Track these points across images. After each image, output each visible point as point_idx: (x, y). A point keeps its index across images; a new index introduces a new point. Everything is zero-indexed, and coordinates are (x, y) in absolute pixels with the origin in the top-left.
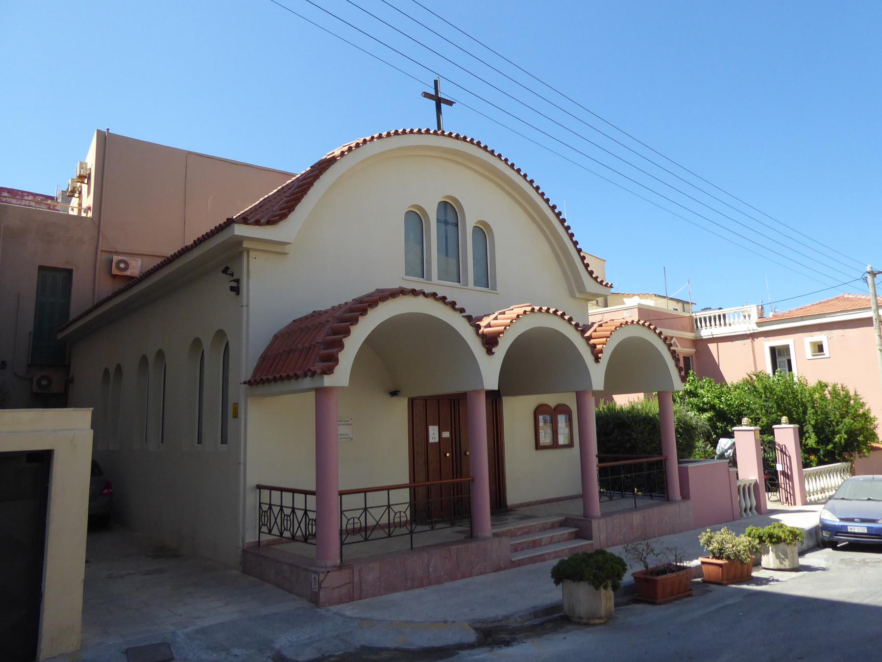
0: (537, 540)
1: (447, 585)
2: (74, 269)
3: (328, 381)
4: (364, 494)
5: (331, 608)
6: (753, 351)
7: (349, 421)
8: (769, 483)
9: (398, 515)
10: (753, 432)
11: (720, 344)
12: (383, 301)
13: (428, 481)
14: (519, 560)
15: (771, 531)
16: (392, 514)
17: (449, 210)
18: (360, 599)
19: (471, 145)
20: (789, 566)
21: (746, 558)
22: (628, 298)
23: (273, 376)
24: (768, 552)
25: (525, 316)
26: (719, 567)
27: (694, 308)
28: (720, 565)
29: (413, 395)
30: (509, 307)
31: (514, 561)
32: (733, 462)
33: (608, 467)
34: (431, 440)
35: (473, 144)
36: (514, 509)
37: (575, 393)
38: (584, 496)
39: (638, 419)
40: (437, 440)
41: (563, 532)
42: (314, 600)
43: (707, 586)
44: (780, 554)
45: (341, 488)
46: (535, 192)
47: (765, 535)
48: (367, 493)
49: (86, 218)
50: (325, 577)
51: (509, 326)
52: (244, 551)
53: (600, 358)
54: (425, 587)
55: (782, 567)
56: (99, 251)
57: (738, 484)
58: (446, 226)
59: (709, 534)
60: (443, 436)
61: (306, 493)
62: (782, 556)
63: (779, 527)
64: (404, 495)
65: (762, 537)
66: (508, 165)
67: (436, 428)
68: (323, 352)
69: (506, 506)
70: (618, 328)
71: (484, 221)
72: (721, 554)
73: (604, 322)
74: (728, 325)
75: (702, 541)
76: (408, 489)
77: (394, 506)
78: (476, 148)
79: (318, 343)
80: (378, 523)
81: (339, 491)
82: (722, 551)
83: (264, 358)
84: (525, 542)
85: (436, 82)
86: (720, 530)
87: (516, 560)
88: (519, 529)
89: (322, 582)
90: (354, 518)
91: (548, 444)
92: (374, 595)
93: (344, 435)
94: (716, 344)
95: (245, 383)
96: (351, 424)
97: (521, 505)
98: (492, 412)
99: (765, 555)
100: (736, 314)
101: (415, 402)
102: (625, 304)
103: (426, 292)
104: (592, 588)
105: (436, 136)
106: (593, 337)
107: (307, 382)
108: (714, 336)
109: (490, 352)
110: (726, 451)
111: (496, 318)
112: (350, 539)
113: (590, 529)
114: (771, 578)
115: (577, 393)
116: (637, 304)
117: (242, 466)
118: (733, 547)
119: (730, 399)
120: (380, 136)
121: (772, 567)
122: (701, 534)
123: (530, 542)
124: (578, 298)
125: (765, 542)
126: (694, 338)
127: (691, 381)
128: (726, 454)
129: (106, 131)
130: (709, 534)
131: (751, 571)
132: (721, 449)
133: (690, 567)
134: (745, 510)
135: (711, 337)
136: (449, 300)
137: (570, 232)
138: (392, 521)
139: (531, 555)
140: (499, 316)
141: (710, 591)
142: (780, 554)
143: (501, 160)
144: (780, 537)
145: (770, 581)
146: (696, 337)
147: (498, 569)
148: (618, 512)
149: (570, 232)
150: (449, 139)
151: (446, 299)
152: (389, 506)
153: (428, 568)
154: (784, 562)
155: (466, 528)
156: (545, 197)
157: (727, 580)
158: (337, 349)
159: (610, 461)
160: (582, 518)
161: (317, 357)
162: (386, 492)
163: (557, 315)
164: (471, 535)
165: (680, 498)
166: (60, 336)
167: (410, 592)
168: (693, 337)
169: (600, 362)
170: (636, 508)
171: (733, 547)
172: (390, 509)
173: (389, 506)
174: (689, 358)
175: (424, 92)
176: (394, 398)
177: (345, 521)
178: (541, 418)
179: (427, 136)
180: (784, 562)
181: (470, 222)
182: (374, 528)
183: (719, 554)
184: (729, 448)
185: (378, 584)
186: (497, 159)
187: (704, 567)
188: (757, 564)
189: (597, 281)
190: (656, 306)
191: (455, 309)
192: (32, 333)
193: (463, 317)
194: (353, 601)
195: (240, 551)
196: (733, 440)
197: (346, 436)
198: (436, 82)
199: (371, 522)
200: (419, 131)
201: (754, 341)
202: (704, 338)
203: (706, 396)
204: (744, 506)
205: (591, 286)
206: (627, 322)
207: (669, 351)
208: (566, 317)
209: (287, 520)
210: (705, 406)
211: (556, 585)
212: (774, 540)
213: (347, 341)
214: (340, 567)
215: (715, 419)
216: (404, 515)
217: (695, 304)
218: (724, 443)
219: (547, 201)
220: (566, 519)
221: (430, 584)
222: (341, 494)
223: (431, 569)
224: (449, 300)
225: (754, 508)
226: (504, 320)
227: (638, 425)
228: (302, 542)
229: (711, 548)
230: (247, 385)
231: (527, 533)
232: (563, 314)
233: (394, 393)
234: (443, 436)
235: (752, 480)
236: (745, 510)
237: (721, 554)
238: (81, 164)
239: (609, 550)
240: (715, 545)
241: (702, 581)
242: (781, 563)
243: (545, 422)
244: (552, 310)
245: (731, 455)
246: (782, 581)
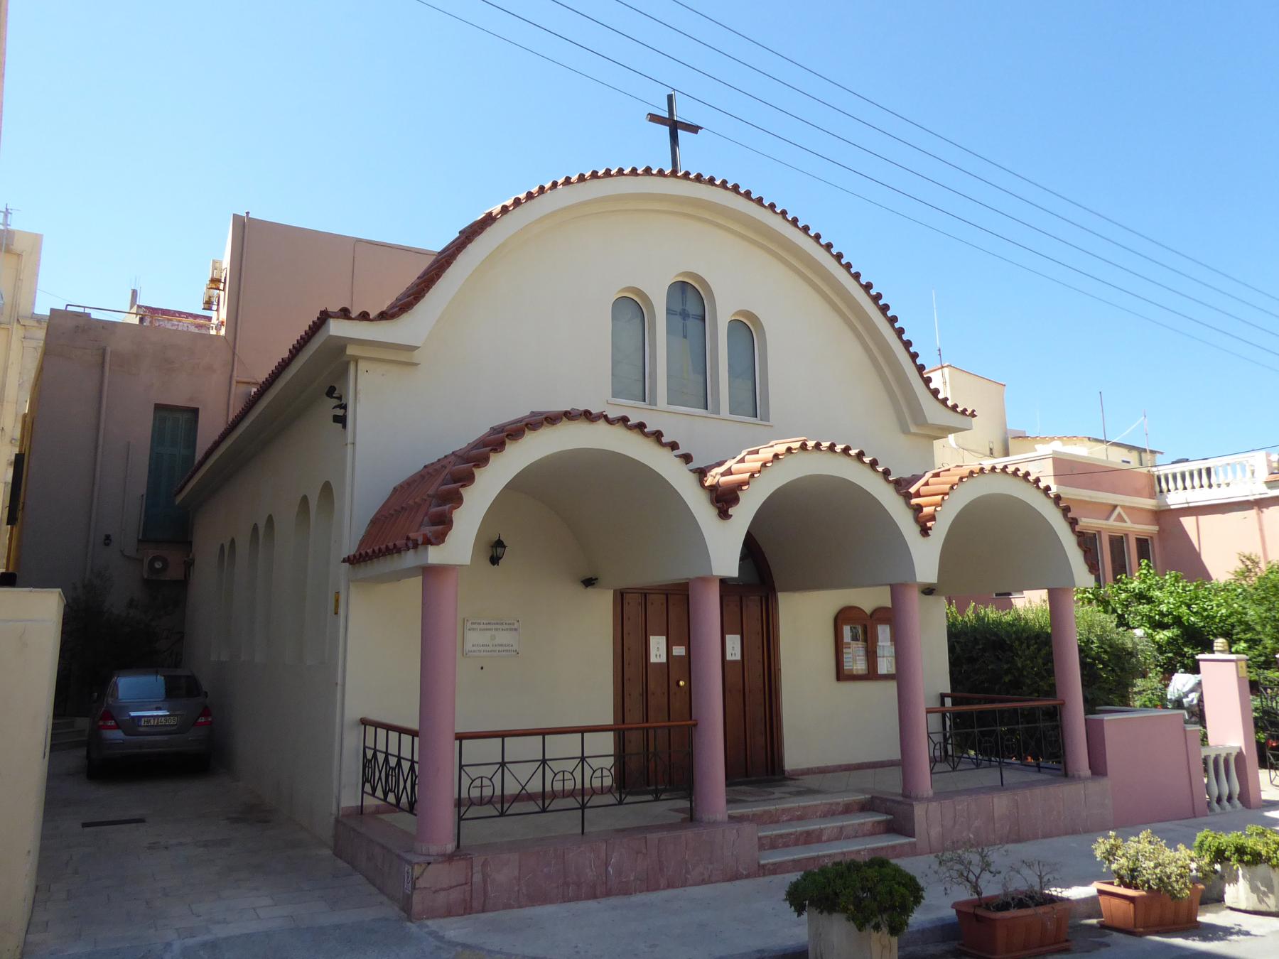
0: (813, 831)
1: (638, 898)
2: (200, 407)
3: (435, 555)
4: (541, 737)
5: (429, 923)
6: (1261, 530)
7: (513, 624)
8: (1272, 754)
9: (560, 777)
10: (1233, 664)
11: (1201, 518)
12: (534, 430)
13: (647, 721)
14: (774, 864)
15: (1241, 841)
16: (549, 775)
17: (690, 293)
18: (483, 911)
19: (722, 191)
20: (1276, 906)
21: (1181, 889)
22: (1043, 443)
23: (371, 550)
24: (1236, 880)
25: (791, 456)
26: (1128, 902)
27: (1158, 458)
28: (1131, 899)
29: (623, 584)
30: (769, 443)
31: (764, 866)
32: (1198, 714)
33: (972, 712)
34: (653, 659)
35: (727, 188)
36: (796, 777)
37: (888, 588)
38: (904, 763)
39: (1025, 635)
40: (664, 660)
41: (862, 821)
42: (406, 908)
43: (1106, 936)
44: (1259, 885)
45: (460, 729)
46: (835, 263)
47: (1229, 848)
48: (464, 742)
49: (217, 336)
50: (423, 872)
51: (759, 472)
52: (337, 821)
53: (930, 528)
54: (599, 900)
55: (1263, 908)
56: (234, 382)
57: (1205, 752)
58: (684, 319)
59: (1112, 841)
60: (674, 654)
61: (401, 731)
62: (1263, 889)
63: (1257, 834)
64: (605, 743)
65: (1225, 850)
66: (788, 221)
68: (434, 510)
69: (783, 771)
70: (964, 480)
71: (748, 311)
72: (1133, 878)
73: (943, 469)
74: (1215, 487)
75: (1099, 854)
76: (611, 734)
77: (590, 759)
78: (731, 195)
79: (429, 496)
80: (523, 788)
81: (456, 734)
82: (1136, 874)
83: (374, 522)
84: (791, 834)
85: (670, 98)
86: (1137, 835)
87: (768, 864)
88: (784, 811)
89: (418, 878)
90: (482, 778)
91: (860, 672)
92: (508, 906)
94: (1194, 518)
95: (344, 561)
96: (516, 630)
97: (809, 772)
98: (760, 618)
99: (1232, 885)
100: (1229, 468)
101: (627, 598)
102: (1036, 451)
103: (609, 416)
104: (852, 926)
105: (662, 178)
106: (922, 494)
107: (410, 559)
108: (1191, 505)
109: (724, 514)
110: (1186, 695)
111: (742, 461)
112: (473, 812)
113: (910, 818)
114: (1237, 928)
115: (892, 586)
116: (1051, 452)
117: (339, 687)
118: (1156, 867)
119: (1209, 607)
120: (568, 181)
121: (1243, 907)
122: (1095, 841)
123: (801, 833)
124: (915, 434)
125: (1230, 861)
126: (1154, 508)
127: (1142, 576)
128: (1185, 700)
129: (245, 215)
130: (1112, 841)
131: (1197, 912)
132: (1176, 691)
133: (1068, 899)
134: (1219, 800)
135: (1186, 505)
137: (897, 325)
138: (548, 788)
139: (796, 857)
140: (748, 458)
141: (1108, 945)
142: (1259, 885)
143: (775, 212)
144: (1259, 854)
145: (1232, 934)
146: (1159, 507)
147: (736, 877)
148: (969, 792)
149: (897, 325)
150: (685, 182)
151: (645, 427)
152: (583, 759)
153: (607, 868)
154: (1266, 899)
155: (685, 804)
156: (853, 270)
157: (1144, 928)
158: (450, 505)
159: (979, 703)
160: (900, 799)
161: (426, 518)
162: (500, 740)
163: (850, 455)
164: (691, 818)
165: (1089, 773)
166: (179, 499)
167: (572, 905)
168: (1153, 506)
169: (929, 535)
170: (1002, 786)
171: (1156, 867)
172: (585, 763)
173: (544, 762)
174: (1146, 540)
175: (649, 114)
176: (590, 589)
177: (466, 782)
178: (847, 630)
179: (647, 178)
180: (1266, 899)
181: (724, 312)
182: (517, 798)
183: (1130, 878)
184: (1192, 691)
185: (516, 889)
186: (769, 213)
187: (1102, 899)
188: (1215, 899)
189: (947, 406)
190: (1090, 455)
191: (663, 445)
192: (145, 497)
193: (676, 456)
194: (470, 914)
195: (332, 820)
196: (1198, 677)
197: (508, 648)
198: (670, 98)
199: (512, 788)
200: (620, 172)
201: (1262, 512)
202: (1172, 507)
203: (1166, 601)
204: (1215, 792)
205: (934, 413)
206: (972, 473)
207: (1066, 520)
208: (867, 460)
209: (392, 775)
210: (1166, 620)
211: (799, 916)
212: (1246, 858)
213: (468, 494)
214: (450, 858)
215: (1181, 641)
216: (571, 777)
217: (1162, 453)
218: (1181, 682)
219: (857, 276)
220: (872, 797)
221: (608, 894)
222: (460, 737)
223: (610, 869)
225: (1236, 796)
226: (753, 463)
227: (1024, 646)
228: (406, 811)
229: (1114, 867)
230: (347, 564)
231: (800, 818)
232: (860, 455)
233: (589, 582)
234: (674, 654)
235: (1232, 748)
236: (1219, 800)
237: (1133, 878)
238: (214, 262)
239: (893, 861)
240: (1121, 863)
241: (1099, 926)
242: (1261, 901)
243: (855, 638)
244: (839, 448)
245: (1195, 702)
246: (1256, 936)
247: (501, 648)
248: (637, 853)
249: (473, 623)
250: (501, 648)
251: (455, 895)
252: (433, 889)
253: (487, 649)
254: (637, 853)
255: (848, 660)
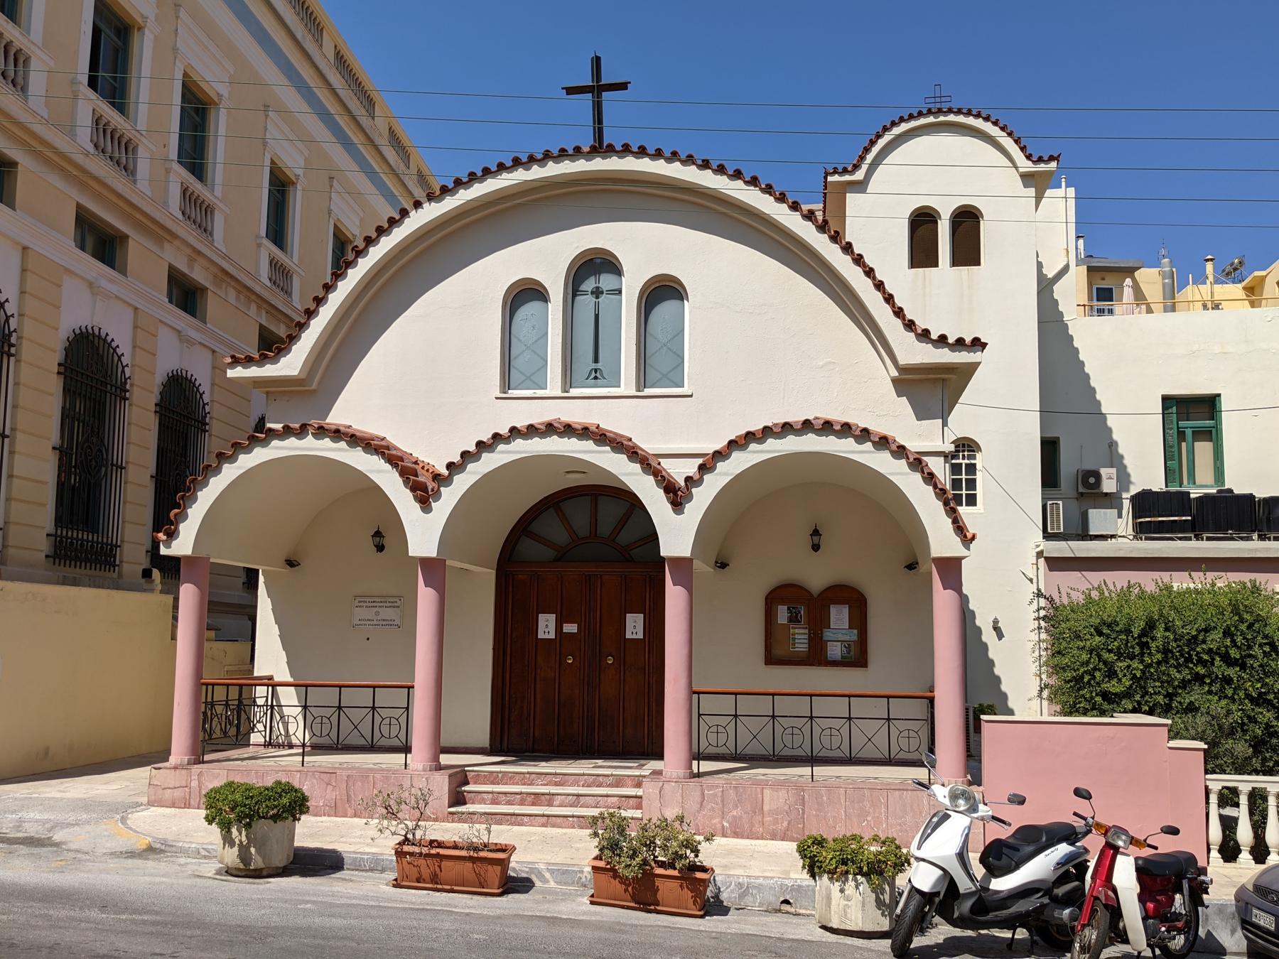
7: (396, 602)
9: (319, 720)
16: (378, 719)
40: (552, 636)
48: (813, 697)
67: (552, 617)
93: (387, 620)
96: (399, 607)
136: (456, 458)
197: (391, 623)
224: (456, 458)
247: (384, 623)
248: (327, 785)
249: (360, 602)
250: (384, 623)
251: (178, 794)
252: (163, 787)
253: (372, 623)
254: (327, 785)
255: (803, 637)
